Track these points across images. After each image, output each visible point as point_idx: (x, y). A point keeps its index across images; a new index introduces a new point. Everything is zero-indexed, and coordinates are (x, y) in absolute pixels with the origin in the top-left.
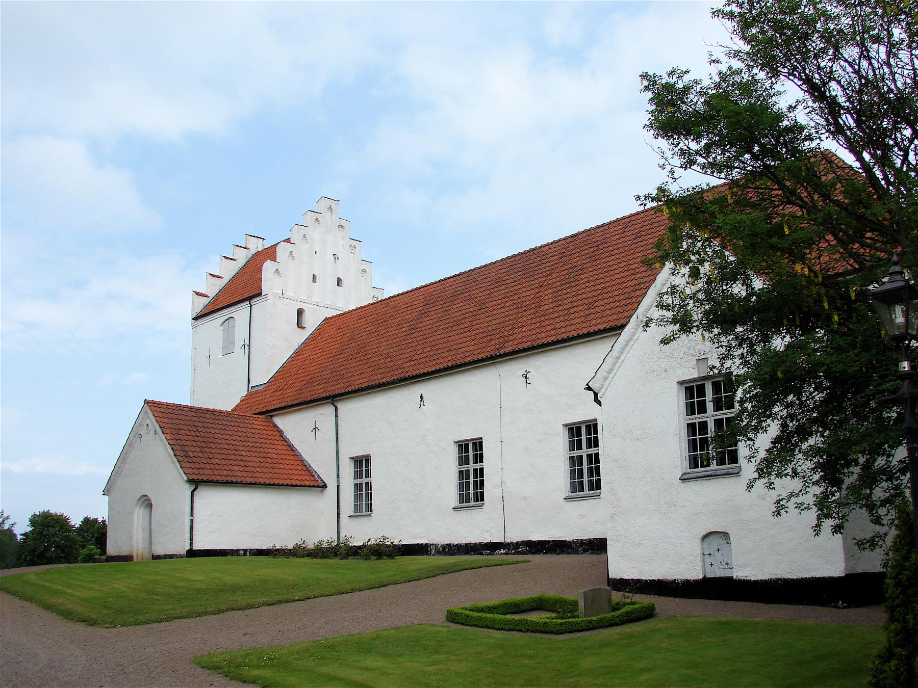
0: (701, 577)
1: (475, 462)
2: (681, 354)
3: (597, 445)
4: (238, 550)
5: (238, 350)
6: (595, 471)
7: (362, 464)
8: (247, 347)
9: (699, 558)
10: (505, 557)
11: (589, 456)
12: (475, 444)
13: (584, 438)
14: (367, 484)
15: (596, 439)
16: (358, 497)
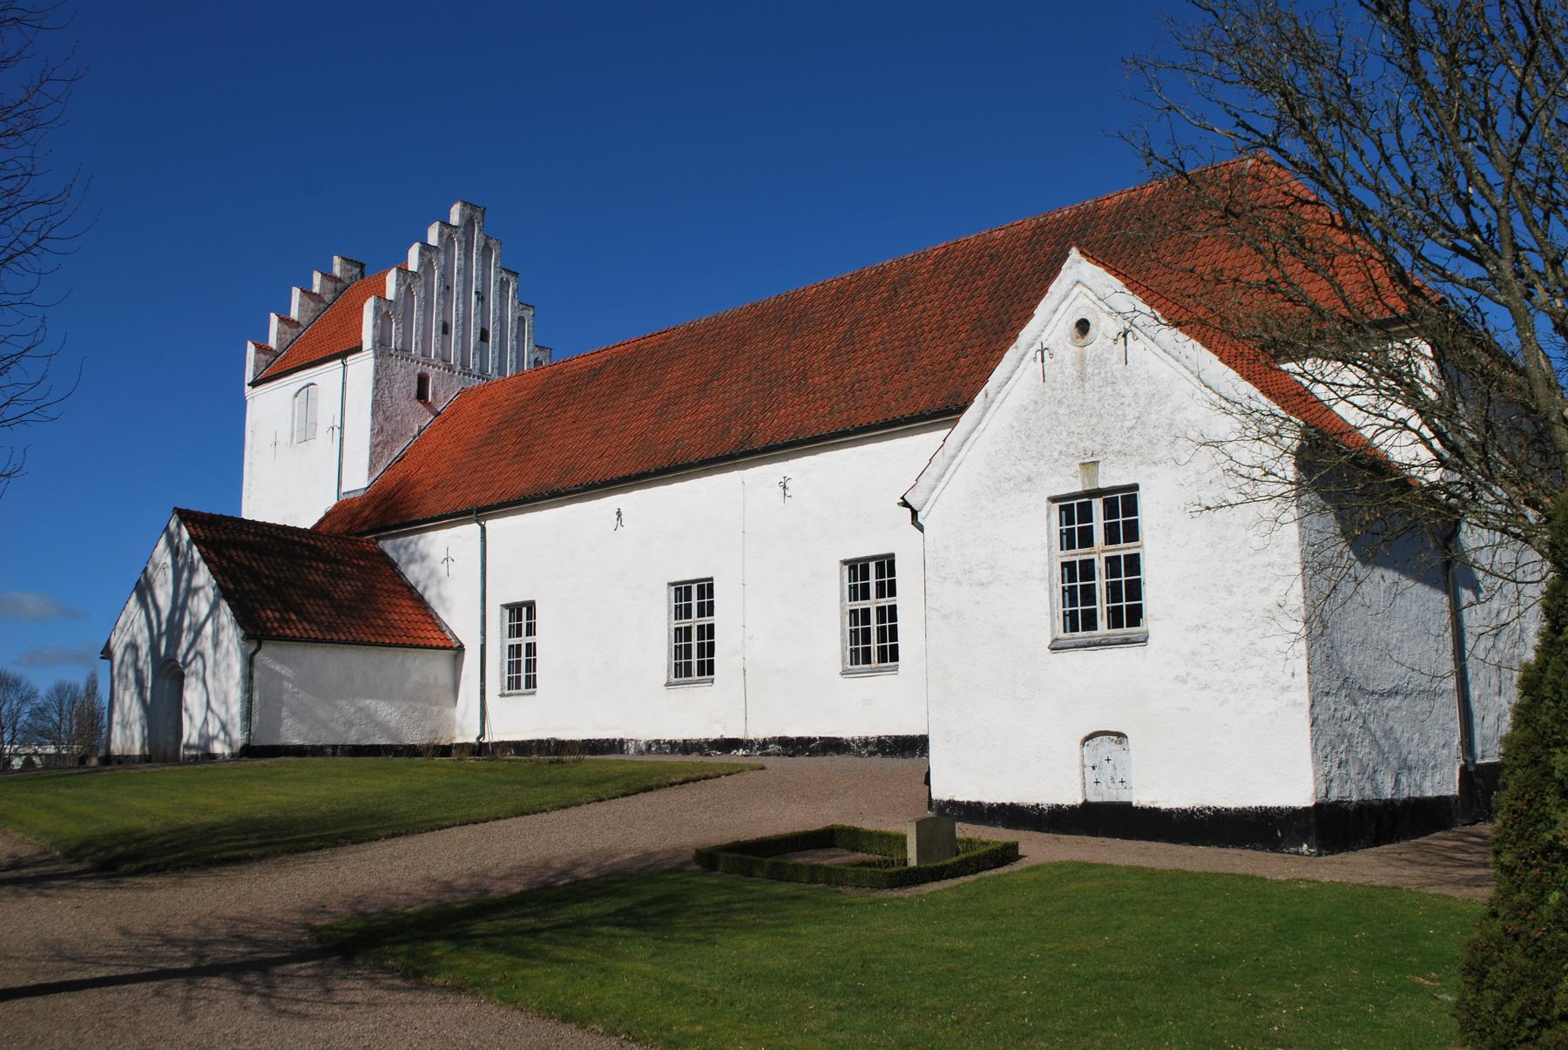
0: (1080, 801)
1: (701, 614)
2: (1056, 454)
3: (893, 593)
4: (322, 747)
5: (322, 428)
6: (708, 650)
7: (521, 615)
8: (337, 432)
9: (1078, 771)
10: (747, 760)
11: (881, 610)
12: (701, 588)
13: (873, 581)
14: (528, 645)
15: (711, 604)
16: (514, 667)
